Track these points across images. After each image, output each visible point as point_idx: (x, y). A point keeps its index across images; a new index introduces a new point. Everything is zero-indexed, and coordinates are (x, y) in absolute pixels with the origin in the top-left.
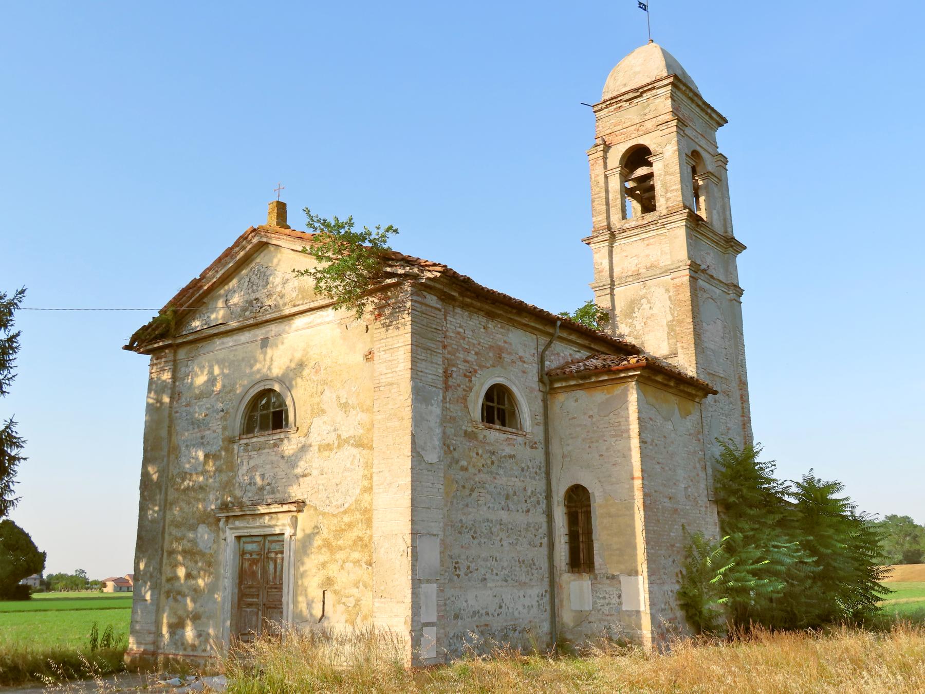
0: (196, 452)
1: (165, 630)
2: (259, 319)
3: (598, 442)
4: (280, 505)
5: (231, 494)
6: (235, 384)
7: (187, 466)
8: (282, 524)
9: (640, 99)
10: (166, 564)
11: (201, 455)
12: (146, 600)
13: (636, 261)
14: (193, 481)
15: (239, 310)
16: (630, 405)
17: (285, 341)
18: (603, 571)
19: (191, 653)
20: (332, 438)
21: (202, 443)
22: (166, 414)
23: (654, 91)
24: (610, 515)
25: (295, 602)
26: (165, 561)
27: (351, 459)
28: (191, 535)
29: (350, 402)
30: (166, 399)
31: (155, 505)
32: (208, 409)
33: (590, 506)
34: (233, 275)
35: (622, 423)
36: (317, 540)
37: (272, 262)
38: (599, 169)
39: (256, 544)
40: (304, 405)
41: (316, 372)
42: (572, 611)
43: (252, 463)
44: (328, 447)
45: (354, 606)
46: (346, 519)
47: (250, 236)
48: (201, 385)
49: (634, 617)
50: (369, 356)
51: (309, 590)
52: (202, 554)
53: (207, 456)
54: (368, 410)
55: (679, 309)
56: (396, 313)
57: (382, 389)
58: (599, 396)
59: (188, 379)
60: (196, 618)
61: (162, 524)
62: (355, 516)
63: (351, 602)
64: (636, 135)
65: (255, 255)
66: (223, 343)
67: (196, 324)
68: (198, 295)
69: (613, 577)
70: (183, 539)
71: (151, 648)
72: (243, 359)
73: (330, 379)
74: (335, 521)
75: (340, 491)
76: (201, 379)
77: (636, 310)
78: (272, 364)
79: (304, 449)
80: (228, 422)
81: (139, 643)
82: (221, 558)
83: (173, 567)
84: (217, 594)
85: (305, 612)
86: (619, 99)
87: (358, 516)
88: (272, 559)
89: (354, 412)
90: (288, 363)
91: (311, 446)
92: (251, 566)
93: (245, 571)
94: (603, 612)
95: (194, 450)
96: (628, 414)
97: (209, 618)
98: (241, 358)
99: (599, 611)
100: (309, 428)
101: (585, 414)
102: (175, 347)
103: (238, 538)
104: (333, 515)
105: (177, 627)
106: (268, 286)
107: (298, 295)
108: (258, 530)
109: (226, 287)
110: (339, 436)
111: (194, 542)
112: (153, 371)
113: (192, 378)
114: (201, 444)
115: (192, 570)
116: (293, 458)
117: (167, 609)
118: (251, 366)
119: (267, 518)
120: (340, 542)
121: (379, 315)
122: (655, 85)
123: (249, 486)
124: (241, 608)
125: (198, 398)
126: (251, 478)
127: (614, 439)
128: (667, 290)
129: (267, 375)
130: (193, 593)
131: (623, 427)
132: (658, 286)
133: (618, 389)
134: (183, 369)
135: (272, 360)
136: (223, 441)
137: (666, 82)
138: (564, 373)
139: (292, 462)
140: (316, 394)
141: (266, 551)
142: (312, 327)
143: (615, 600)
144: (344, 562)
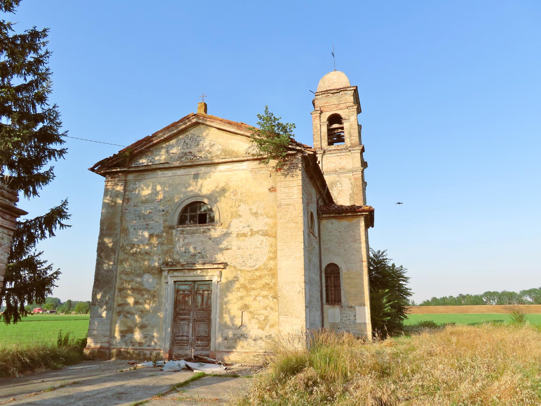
0: (142, 232)
1: (117, 335)
2: (195, 163)
3: (344, 244)
4: (212, 265)
5: (171, 257)
6: (174, 197)
7: (135, 240)
8: (213, 275)
9: (338, 94)
10: (117, 296)
11: (146, 234)
12: (102, 317)
13: (334, 165)
14: (140, 249)
15: (177, 157)
16: (361, 228)
17: (212, 176)
18: (346, 304)
19: (139, 348)
20: (246, 230)
21: (147, 228)
22: (119, 209)
23: (346, 92)
24: (350, 278)
25: (221, 317)
26: (116, 294)
27: (260, 242)
28: (139, 279)
29: (259, 212)
30: (119, 201)
31: (110, 261)
32: (152, 209)
33: (339, 273)
34: (172, 138)
35: (357, 236)
36: (237, 284)
37: (202, 133)
38: (317, 121)
39: (188, 286)
40: (226, 212)
41: (235, 195)
42: (329, 323)
43: (186, 241)
44: (244, 235)
45: (264, 320)
46: (257, 273)
47: (191, 118)
48: (146, 195)
49: (363, 326)
50: (272, 190)
51: (232, 311)
52: (148, 291)
53: (151, 236)
54: (274, 217)
55: (356, 188)
56: (292, 169)
57: (282, 207)
58: (344, 223)
59: (136, 191)
60: (142, 327)
61: (115, 273)
62: (264, 272)
63: (262, 318)
64: (336, 109)
65: (190, 129)
66: (164, 174)
67: (144, 161)
68: (149, 145)
69: (351, 307)
70: (132, 282)
71: (106, 345)
72: (179, 184)
73: (244, 199)
74: (250, 274)
75: (252, 259)
76: (146, 192)
77: (334, 187)
78: (202, 188)
79: (227, 235)
80: (168, 217)
81: (96, 342)
82: (163, 293)
83: (123, 298)
84: (160, 313)
85: (229, 323)
86: (329, 92)
87: (266, 272)
88: (200, 294)
89: (262, 218)
90: (214, 188)
91: (231, 233)
92: (184, 298)
93: (179, 301)
94: (346, 324)
95: (141, 231)
96: (360, 232)
97: (153, 327)
98: (178, 183)
99: (344, 323)
100: (230, 224)
101: (337, 230)
102: (126, 173)
103: (175, 282)
104: (248, 271)
105: (127, 332)
106: (199, 146)
107: (221, 153)
108: (192, 278)
109: (167, 144)
110: (251, 230)
111: (141, 283)
112: (108, 185)
113: (139, 191)
114: (147, 228)
115: (139, 300)
116: (218, 240)
117: (119, 322)
118: (186, 188)
119: (199, 271)
120: (253, 286)
121: (280, 169)
122: (347, 89)
123: (184, 253)
124: (176, 321)
125: (144, 202)
126: (186, 249)
127: (352, 243)
128: (350, 180)
129: (198, 193)
130: (140, 313)
131: (357, 238)
132: (345, 177)
133: (355, 220)
134: (131, 186)
135: (202, 185)
136: (164, 227)
137: (352, 89)
138: (330, 210)
139: (217, 241)
140: (235, 206)
141: (196, 289)
142: (231, 171)
143: (352, 318)
144: (256, 296)
